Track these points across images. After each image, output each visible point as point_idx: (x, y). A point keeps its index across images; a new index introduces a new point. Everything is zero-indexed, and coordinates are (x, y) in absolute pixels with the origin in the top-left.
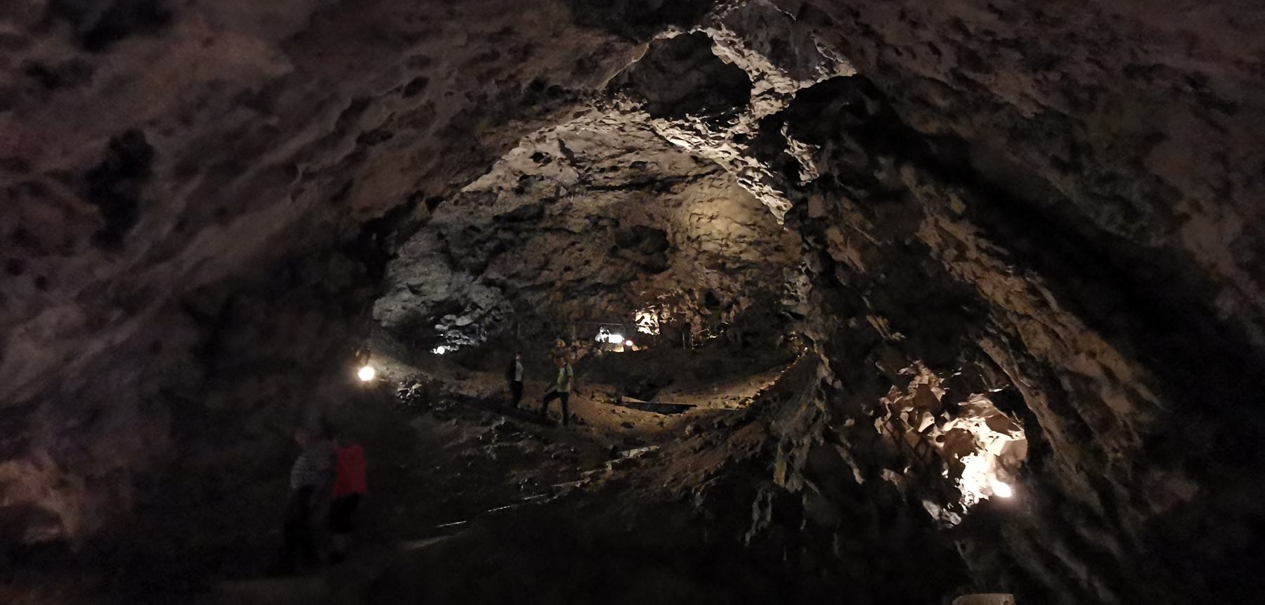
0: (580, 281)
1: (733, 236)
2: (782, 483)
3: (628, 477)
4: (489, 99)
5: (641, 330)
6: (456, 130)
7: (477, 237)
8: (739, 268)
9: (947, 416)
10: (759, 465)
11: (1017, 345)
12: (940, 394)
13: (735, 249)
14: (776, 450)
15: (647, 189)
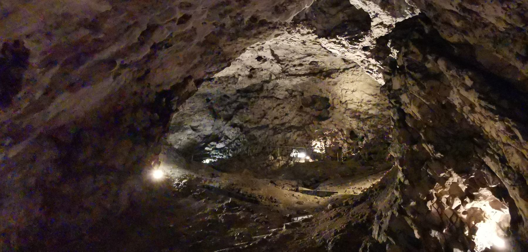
0: (283, 124)
1: (364, 101)
2: (376, 237)
3: (293, 233)
4: (226, 27)
5: (315, 151)
6: (209, 43)
7: (228, 101)
8: (368, 118)
9: (468, 200)
10: (364, 228)
11: (503, 161)
12: (464, 188)
13: (366, 108)
14: (374, 218)
15: (318, 76)
